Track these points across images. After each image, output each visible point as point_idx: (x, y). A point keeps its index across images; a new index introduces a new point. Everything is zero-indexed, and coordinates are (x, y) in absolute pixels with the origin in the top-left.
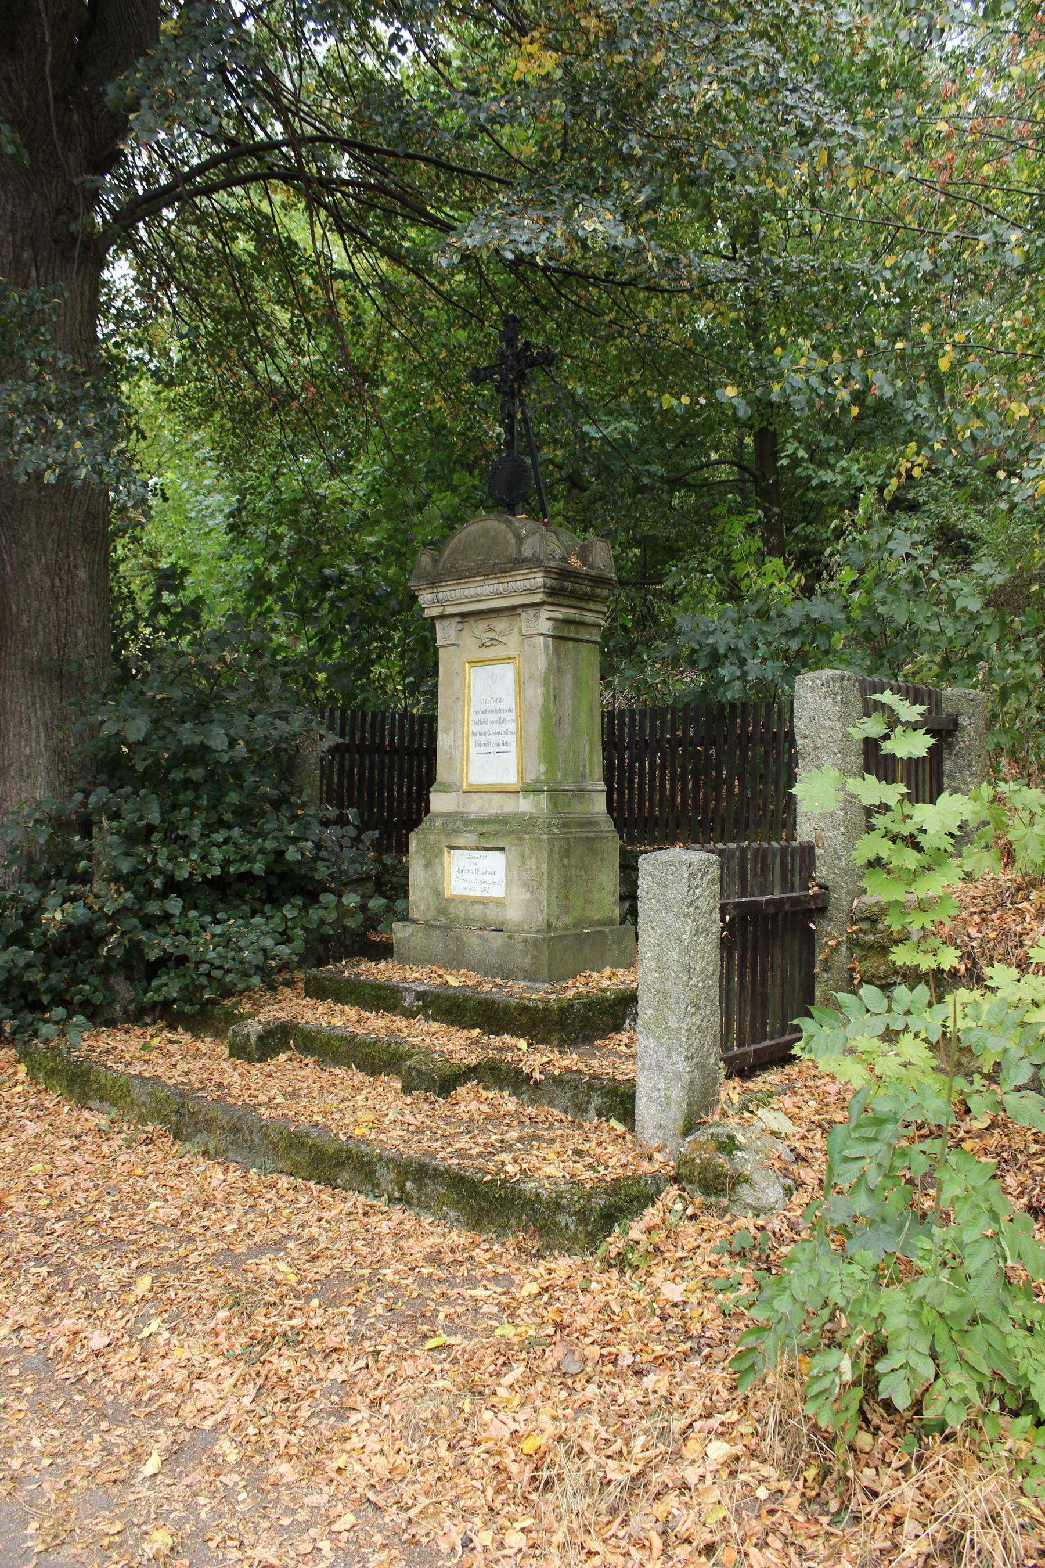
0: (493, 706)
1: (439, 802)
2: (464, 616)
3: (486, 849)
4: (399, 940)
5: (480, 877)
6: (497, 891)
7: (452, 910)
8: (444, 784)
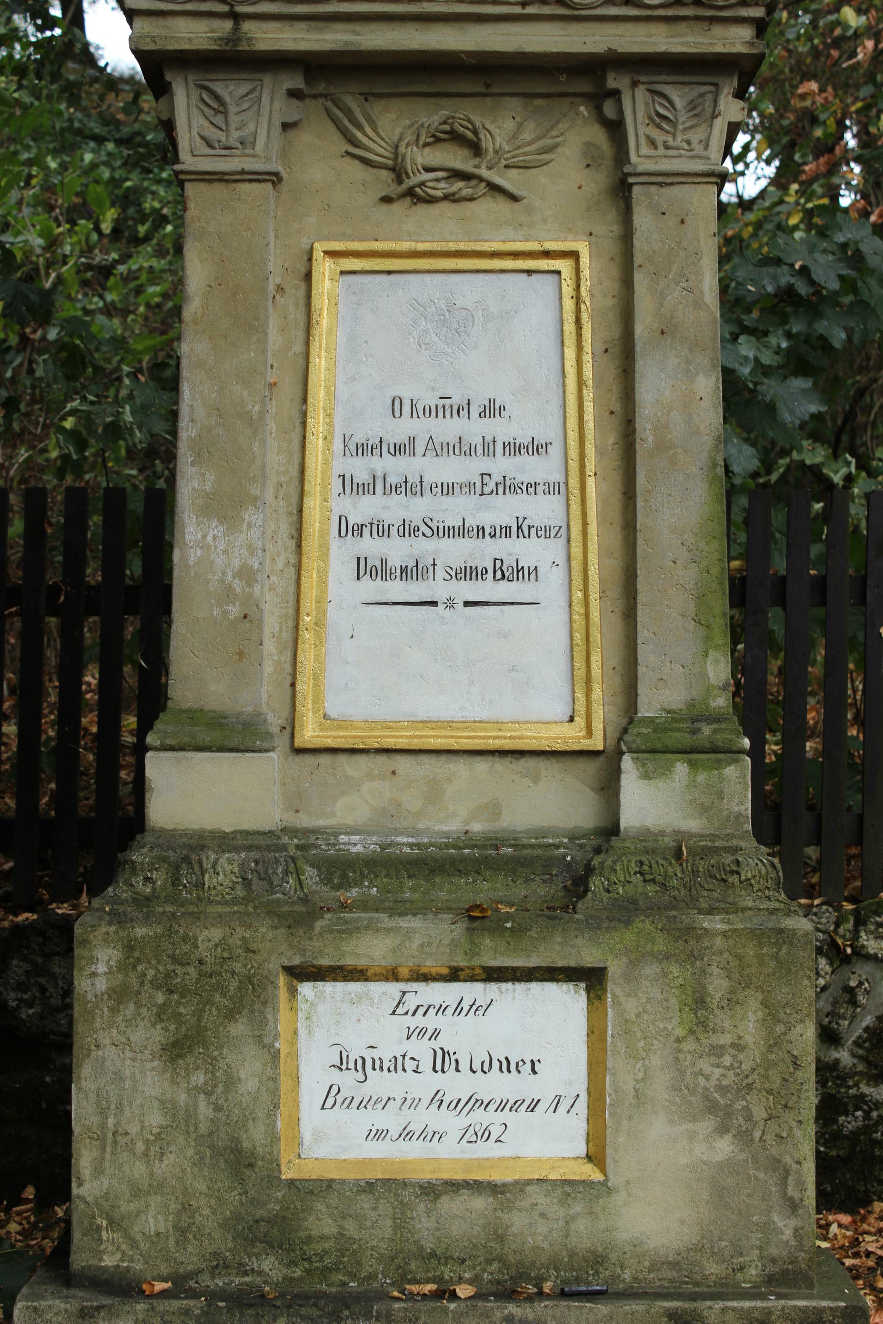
0: (448, 429)
1: (188, 793)
3: (495, 975)
5: (457, 1085)
7: (321, 1223)
8: (194, 716)
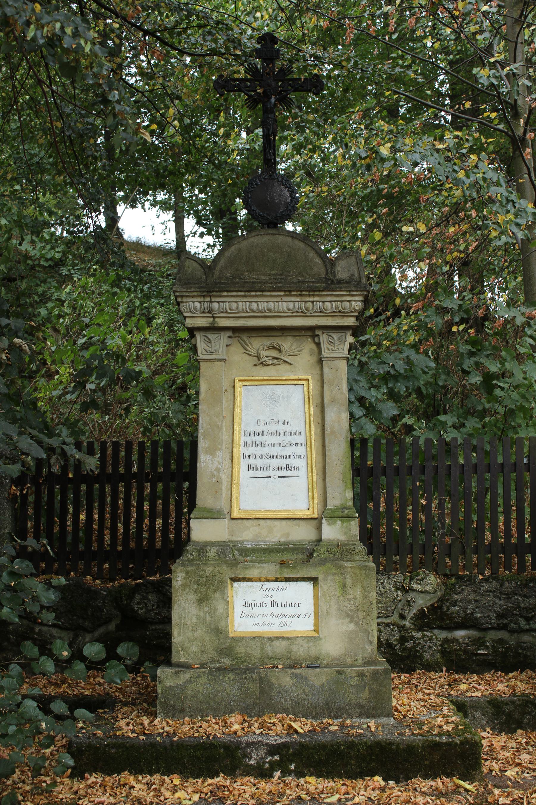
1: (201, 530)
2: (236, 330)
3: (288, 580)
4: (167, 690)
5: (277, 610)
6: (304, 625)
8: (203, 509)
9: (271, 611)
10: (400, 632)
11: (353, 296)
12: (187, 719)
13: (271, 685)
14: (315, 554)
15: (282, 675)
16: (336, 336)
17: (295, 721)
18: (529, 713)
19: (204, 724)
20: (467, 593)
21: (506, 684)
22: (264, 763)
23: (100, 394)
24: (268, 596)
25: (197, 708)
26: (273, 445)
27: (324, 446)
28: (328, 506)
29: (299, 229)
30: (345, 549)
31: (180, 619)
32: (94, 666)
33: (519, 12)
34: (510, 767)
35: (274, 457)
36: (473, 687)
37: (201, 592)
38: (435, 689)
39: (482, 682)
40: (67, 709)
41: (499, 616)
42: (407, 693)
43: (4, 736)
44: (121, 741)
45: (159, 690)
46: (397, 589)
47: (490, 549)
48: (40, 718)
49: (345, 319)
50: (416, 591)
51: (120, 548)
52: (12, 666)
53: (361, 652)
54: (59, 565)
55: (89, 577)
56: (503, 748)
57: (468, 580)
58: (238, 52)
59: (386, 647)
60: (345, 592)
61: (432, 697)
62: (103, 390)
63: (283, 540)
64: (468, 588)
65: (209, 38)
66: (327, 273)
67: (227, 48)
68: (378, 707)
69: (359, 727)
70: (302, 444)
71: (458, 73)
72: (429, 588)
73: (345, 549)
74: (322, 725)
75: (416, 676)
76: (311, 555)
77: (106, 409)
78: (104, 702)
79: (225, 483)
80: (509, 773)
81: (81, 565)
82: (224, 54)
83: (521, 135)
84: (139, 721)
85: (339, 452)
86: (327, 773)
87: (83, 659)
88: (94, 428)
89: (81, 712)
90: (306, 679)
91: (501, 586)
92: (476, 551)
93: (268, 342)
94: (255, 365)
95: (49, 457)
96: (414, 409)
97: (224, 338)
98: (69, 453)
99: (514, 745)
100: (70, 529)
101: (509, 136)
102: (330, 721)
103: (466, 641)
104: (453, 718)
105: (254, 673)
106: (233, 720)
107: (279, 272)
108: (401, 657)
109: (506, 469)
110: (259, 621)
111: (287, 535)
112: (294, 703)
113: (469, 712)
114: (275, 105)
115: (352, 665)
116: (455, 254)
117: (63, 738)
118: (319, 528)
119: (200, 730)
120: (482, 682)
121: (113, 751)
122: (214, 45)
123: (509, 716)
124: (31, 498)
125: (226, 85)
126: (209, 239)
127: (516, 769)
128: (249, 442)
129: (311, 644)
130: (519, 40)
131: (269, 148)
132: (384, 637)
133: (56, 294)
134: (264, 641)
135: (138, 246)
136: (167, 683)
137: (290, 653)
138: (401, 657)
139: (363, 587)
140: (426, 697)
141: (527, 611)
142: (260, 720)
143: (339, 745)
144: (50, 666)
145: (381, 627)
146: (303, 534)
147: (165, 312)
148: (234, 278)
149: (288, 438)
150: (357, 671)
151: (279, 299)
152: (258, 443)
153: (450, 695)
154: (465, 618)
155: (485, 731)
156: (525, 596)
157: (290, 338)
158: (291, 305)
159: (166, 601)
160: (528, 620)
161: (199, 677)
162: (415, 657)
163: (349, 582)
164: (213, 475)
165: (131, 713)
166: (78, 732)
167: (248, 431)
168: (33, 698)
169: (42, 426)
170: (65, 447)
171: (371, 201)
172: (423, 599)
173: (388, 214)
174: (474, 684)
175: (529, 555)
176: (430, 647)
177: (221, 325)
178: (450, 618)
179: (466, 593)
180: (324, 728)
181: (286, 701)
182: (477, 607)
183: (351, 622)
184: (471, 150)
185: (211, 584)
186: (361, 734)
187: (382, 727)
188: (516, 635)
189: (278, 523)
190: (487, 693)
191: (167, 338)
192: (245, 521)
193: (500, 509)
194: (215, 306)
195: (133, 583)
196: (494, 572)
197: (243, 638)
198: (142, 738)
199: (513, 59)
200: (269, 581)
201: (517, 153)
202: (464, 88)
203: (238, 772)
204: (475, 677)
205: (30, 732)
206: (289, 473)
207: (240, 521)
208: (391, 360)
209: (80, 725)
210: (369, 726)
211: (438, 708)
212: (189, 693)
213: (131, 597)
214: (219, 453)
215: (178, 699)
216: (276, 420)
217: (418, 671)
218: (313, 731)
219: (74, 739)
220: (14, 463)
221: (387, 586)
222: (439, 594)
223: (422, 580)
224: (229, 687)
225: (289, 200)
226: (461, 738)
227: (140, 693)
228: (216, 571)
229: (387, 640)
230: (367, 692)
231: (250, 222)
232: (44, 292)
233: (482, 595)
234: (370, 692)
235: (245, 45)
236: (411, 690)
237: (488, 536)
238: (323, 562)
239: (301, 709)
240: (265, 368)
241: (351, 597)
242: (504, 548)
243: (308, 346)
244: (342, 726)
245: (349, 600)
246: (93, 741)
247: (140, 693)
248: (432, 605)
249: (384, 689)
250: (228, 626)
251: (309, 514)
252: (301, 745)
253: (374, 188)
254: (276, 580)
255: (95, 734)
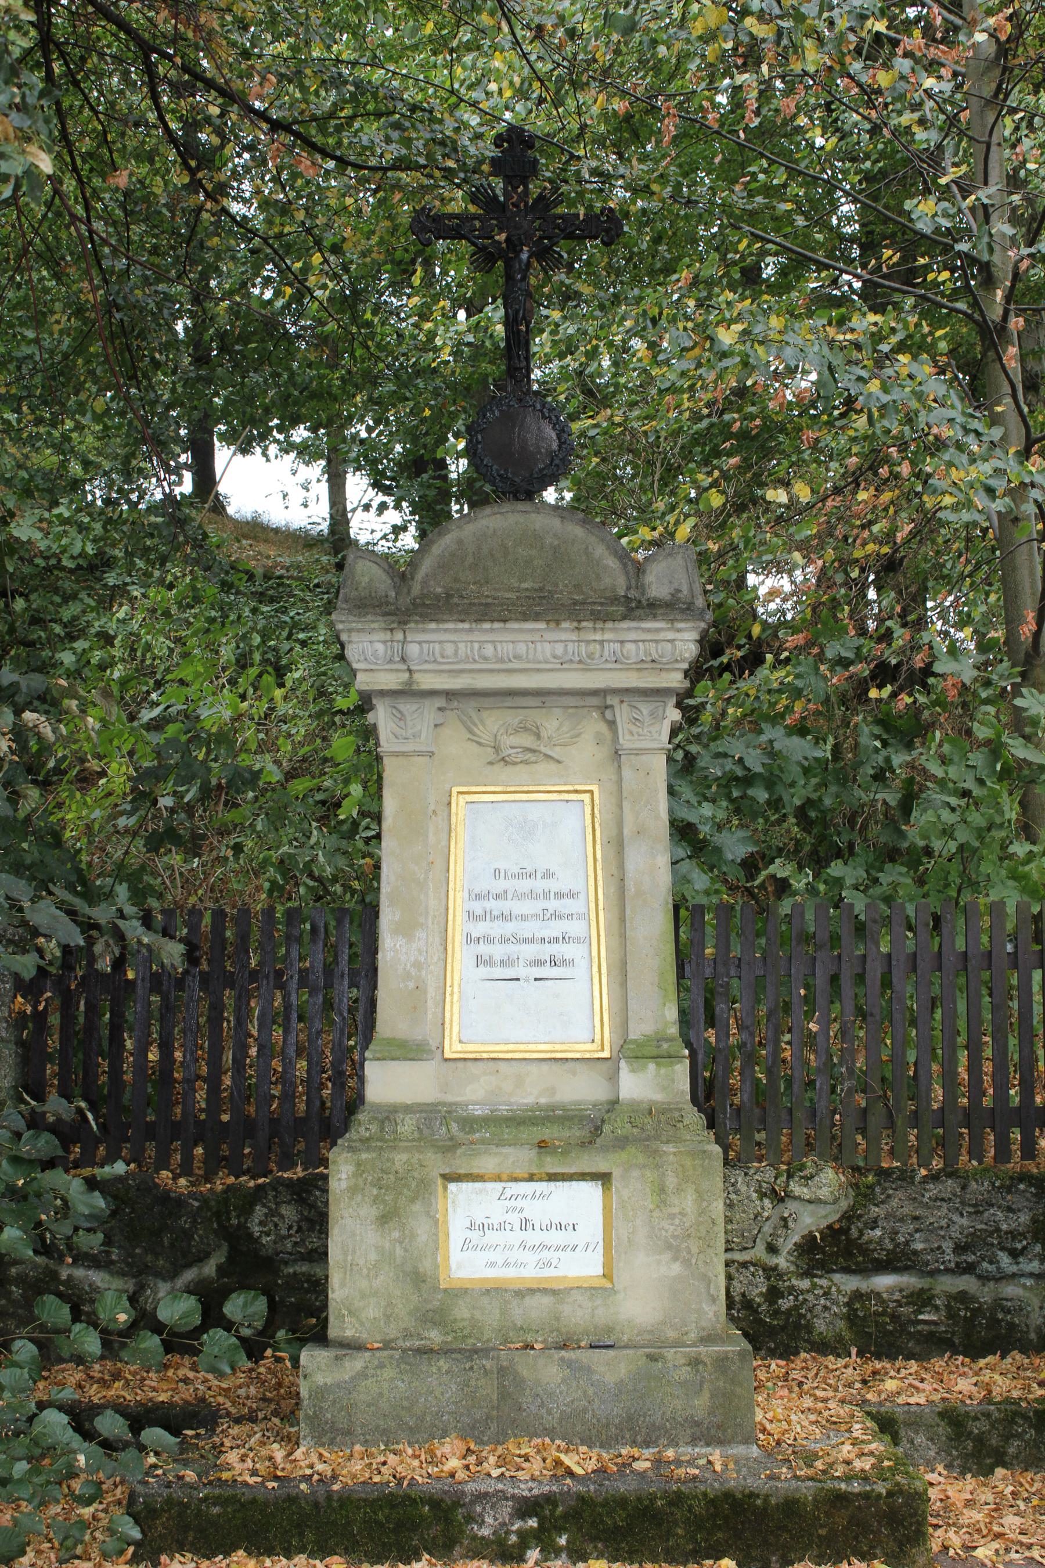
1: (385, 1082)
2: (450, 695)
3: (552, 1177)
4: (319, 1393)
5: (534, 1237)
6: (584, 1265)
8: (390, 1042)
9: (521, 1238)
10: (768, 1278)
11: (679, 630)
12: (358, 1448)
13: (520, 1383)
14: (607, 1128)
15: (541, 1362)
16: (645, 708)
17: (567, 1451)
18: (1019, 1436)
19: (392, 1459)
20: (899, 1202)
21: (974, 1380)
22: (508, 1533)
23: (183, 815)
24: (514, 1209)
25: (377, 1427)
26: (525, 918)
27: (622, 919)
28: (632, 1036)
29: (568, 496)
30: (663, 1118)
31: (345, 1254)
32: (179, 1343)
33: (994, 86)
34: (982, 1541)
35: (526, 941)
36: (912, 1386)
37: (384, 1201)
38: (836, 1390)
39: (927, 1376)
40: (126, 1429)
41: (960, 1249)
42: (782, 1398)
43: (2, 1482)
44: (230, 1492)
45: (304, 1393)
46: (762, 1195)
47: (941, 1117)
48: (75, 1445)
49: (664, 674)
50: (795, 1198)
51: (225, 1118)
52: (17, 1344)
53: (694, 1317)
54: (107, 1149)
55: (164, 1173)
56: (969, 1503)
57: (898, 1179)
58: (451, 164)
59: (739, 1308)
60: (664, 1202)
61: (832, 1404)
62: (190, 809)
63: (543, 1101)
64: (900, 1194)
65: (395, 135)
66: (629, 588)
67: (429, 156)
68: (725, 1426)
69: (691, 1463)
70: (580, 916)
71: (876, 199)
72: (824, 1193)
73: (663, 1118)
74: (619, 1460)
75: (798, 1363)
76: (597, 1130)
77: (193, 846)
78: (194, 1415)
79: (431, 992)
80: (980, 1553)
81: (151, 1150)
82: (425, 167)
83: (998, 320)
84: (264, 1452)
85: (653, 928)
86: (630, 1552)
87: (158, 1328)
88: (173, 880)
89: (153, 1435)
90: (589, 1370)
91: (964, 1188)
92: (915, 1119)
93: (513, 718)
94: (491, 763)
95: (90, 941)
96: (791, 846)
97: (429, 710)
98: (129, 935)
99: (990, 1498)
100: (128, 1077)
101: (975, 322)
102: (635, 1452)
103: (897, 1296)
104: (873, 1446)
105: (487, 1357)
106: (447, 1449)
107: (537, 586)
108: (769, 1327)
109: (973, 963)
110: (498, 1257)
111: (552, 1091)
112: (564, 1417)
113: (902, 1433)
114: (528, 264)
115: (677, 1344)
116: (871, 547)
117: (116, 1485)
118: (613, 1078)
119: (383, 1469)
120: (927, 1376)
121: (216, 1510)
122: (404, 151)
123: (979, 1442)
124: (54, 1020)
125: (431, 225)
126: (393, 517)
127: (995, 1545)
128: (479, 912)
129: (599, 1302)
130: (995, 139)
131: (517, 348)
132: (737, 1288)
133: (96, 624)
134: (507, 1296)
135: (255, 530)
136: (320, 1379)
137: (558, 1319)
138: (769, 1327)
139: (695, 1188)
140: (820, 1405)
141: (1014, 1238)
142: (500, 1450)
143: (652, 1498)
144: (91, 1343)
145: (732, 1270)
146: (583, 1090)
147: (310, 656)
148: (449, 596)
149: (553, 905)
150: (686, 1355)
151: (537, 637)
152: (495, 913)
153: (865, 1401)
154: (893, 1251)
155: (933, 1471)
156: (1010, 1209)
157: (557, 711)
158: (559, 649)
159: (317, 1220)
160: (1015, 1254)
161: (381, 1366)
162: (798, 1326)
163: (671, 1181)
164: (408, 976)
165: (250, 1436)
166: (147, 1474)
167: (477, 891)
168: (60, 1408)
169: (73, 878)
170: (120, 923)
171: (705, 446)
172: (812, 1214)
173: (741, 469)
174: (911, 1380)
175: (1017, 1130)
176: (826, 1308)
177: (424, 687)
178: (864, 1251)
179: (894, 1203)
180: (624, 1465)
181: (549, 1412)
182: (917, 1231)
183: (675, 1259)
184: (901, 348)
185: (405, 1185)
186: (695, 1477)
187: (736, 1463)
188: (992, 1284)
189: (533, 1068)
190: (936, 1397)
191: (313, 708)
192: (469, 1064)
193: (961, 1040)
194: (413, 650)
195: (252, 1184)
196: (950, 1160)
197: (466, 1291)
198: (271, 1485)
199: (980, 176)
200: (516, 1180)
201: (991, 354)
202: (883, 227)
203: (457, 1550)
204: (914, 1366)
205: (49, 1469)
206: (555, 972)
207: (460, 1064)
208: (736, 747)
209: (152, 1459)
210: (709, 1462)
211: (843, 1427)
212: (363, 1397)
213: (247, 1210)
214: (420, 934)
215: (341, 1409)
216: (529, 869)
217: (803, 1355)
218: (601, 1471)
219: (140, 1489)
220: (25, 951)
221: (744, 1189)
222: (844, 1204)
223: (812, 1177)
224: (440, 1386)
225: (555, 446)
226: (889, 1485)
227: (264, 1399)
228: (414, 1161)
229: (743, 1295)
230: (706, 1394)
231: (478, 485)
232: (75, 618)
233: (926, 1206)
234: (712, 1396)
235: (466, 151)
236: (791, 1391)
237: (938, 1092)
238: (621, 1143)
239: (578, 1428)
240: (510, 769)
241: (676, 1210)
242: (969, 1117)
243: (593, 726)
244: (658, 1462)
245: (672, 1217)
246: (178, 1493)
247: (264, 1399)
248: (830, 1227)
249: (739, 1390)
250: (437, 1267)
251: (589, 1050)
252: (581, 1499)
253: (715, 419)
254: (531, 1178)
255: (181, 1478)
